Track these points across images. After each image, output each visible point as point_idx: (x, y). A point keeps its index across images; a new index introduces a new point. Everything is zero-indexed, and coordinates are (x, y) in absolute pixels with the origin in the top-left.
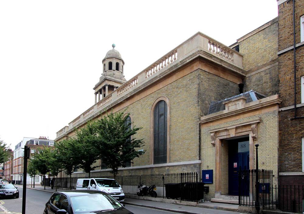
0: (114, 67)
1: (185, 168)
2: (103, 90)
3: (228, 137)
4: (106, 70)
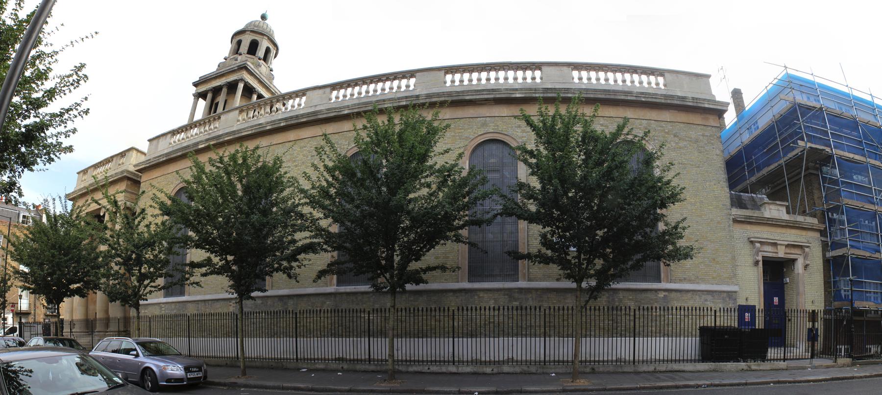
1: (709, 297)
2: (225, 90)
3: (774, 255)
4: (241, 51)
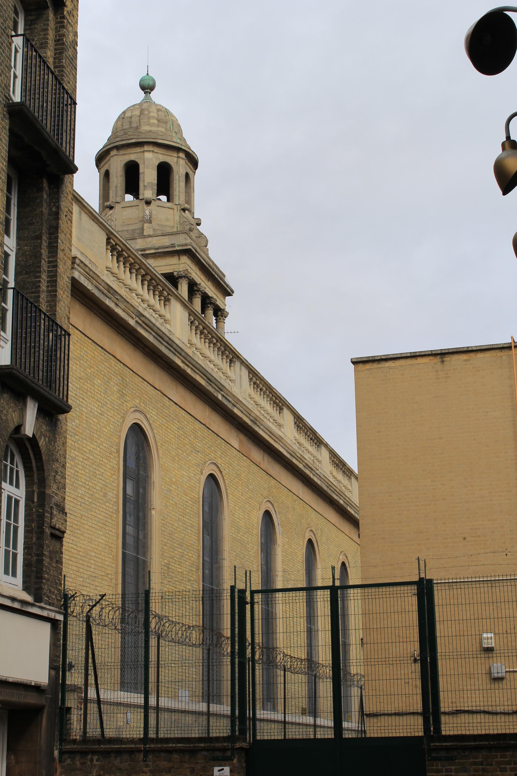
0: (149, 177)
